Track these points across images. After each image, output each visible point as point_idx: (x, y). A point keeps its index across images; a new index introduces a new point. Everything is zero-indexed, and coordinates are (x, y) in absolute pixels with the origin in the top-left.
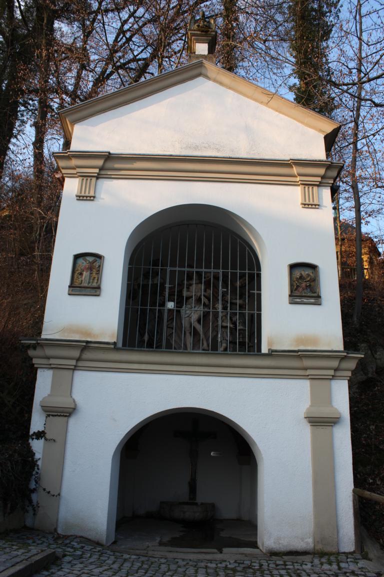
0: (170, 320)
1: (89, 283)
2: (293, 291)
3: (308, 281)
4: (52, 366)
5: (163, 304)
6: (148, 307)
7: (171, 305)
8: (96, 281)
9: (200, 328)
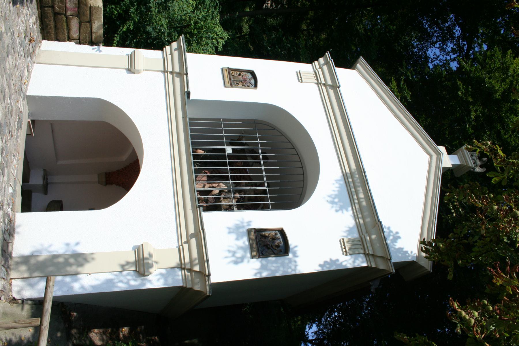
4: (181, 247)
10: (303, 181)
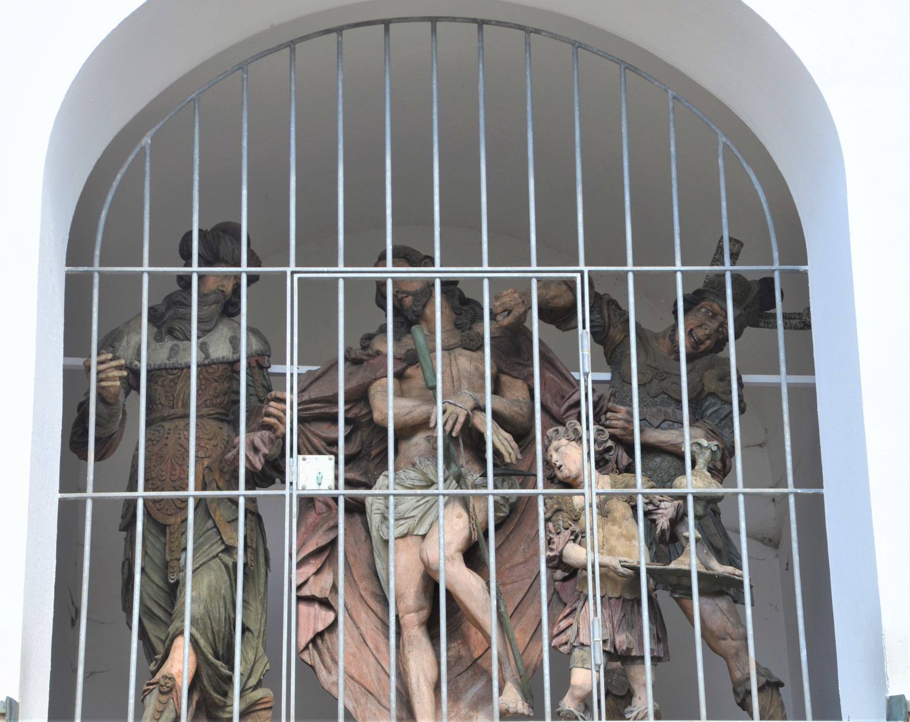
10: (480, 29)
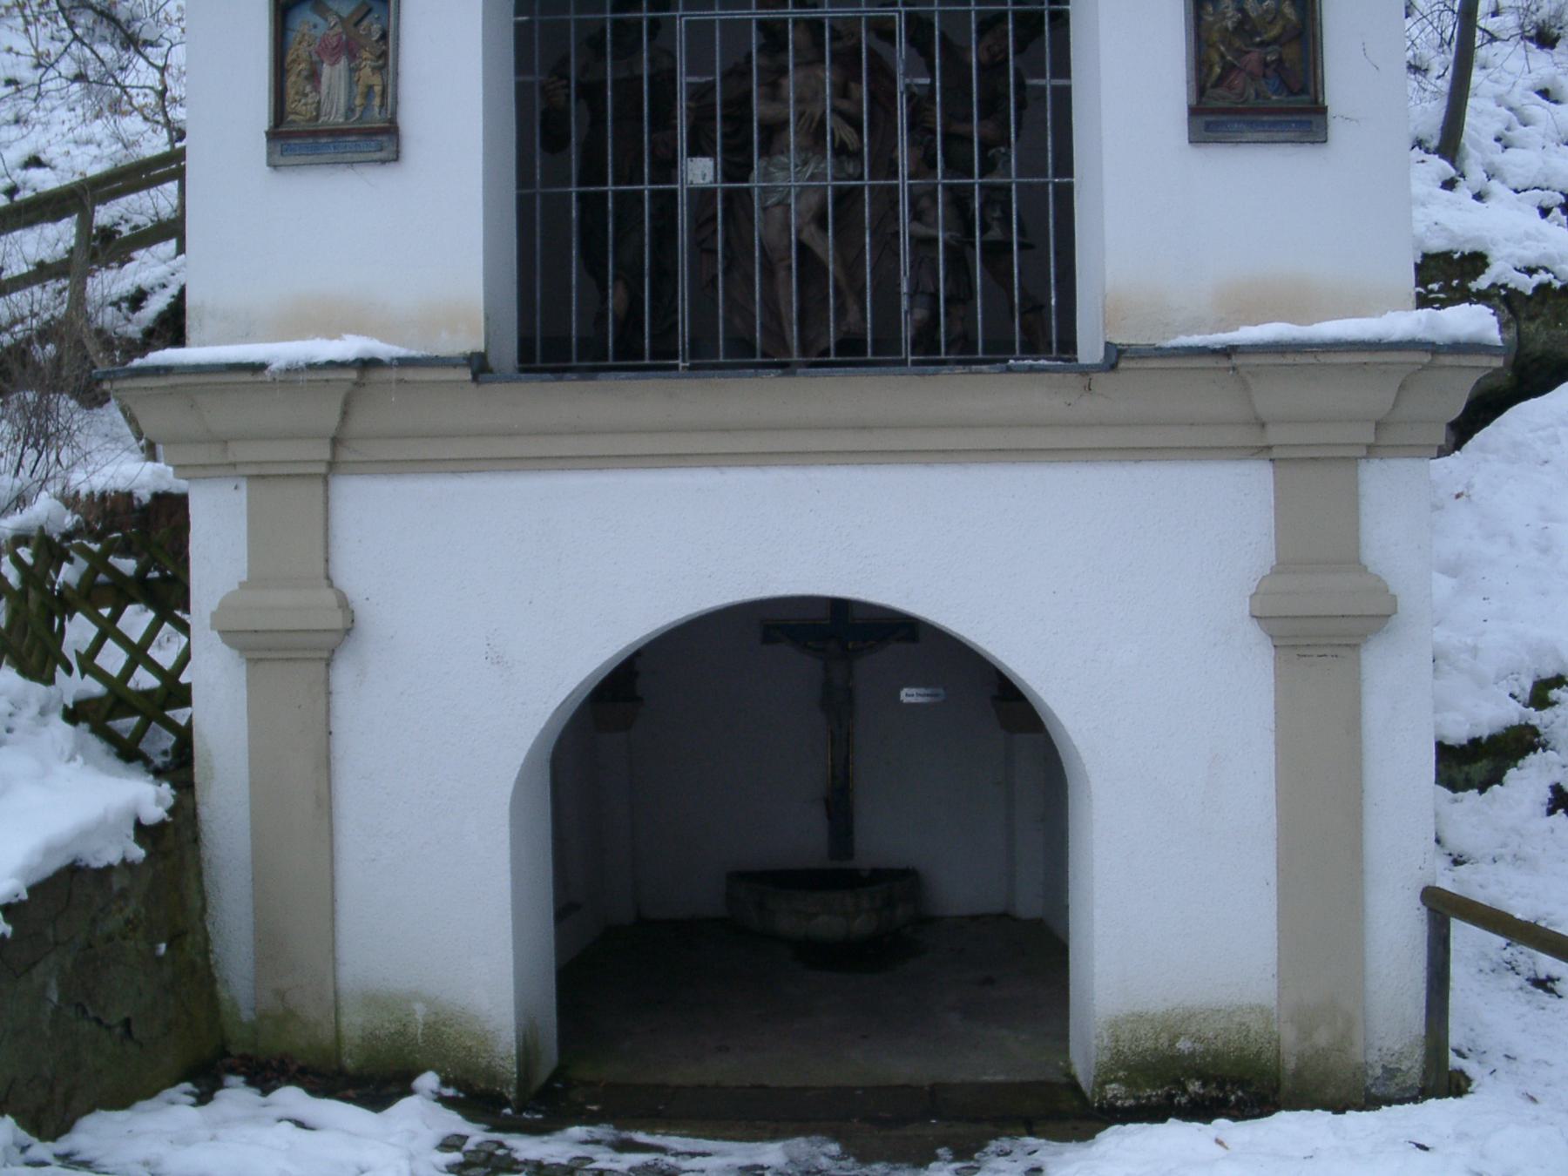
0: (703, 222)
1: (350, 110)
2: (1209, 92)
3: (1275, 41)
5: (666, 168)
6: (610, 188)
7: (700, 171)
8: (377, 101)
9: (827, 248)
